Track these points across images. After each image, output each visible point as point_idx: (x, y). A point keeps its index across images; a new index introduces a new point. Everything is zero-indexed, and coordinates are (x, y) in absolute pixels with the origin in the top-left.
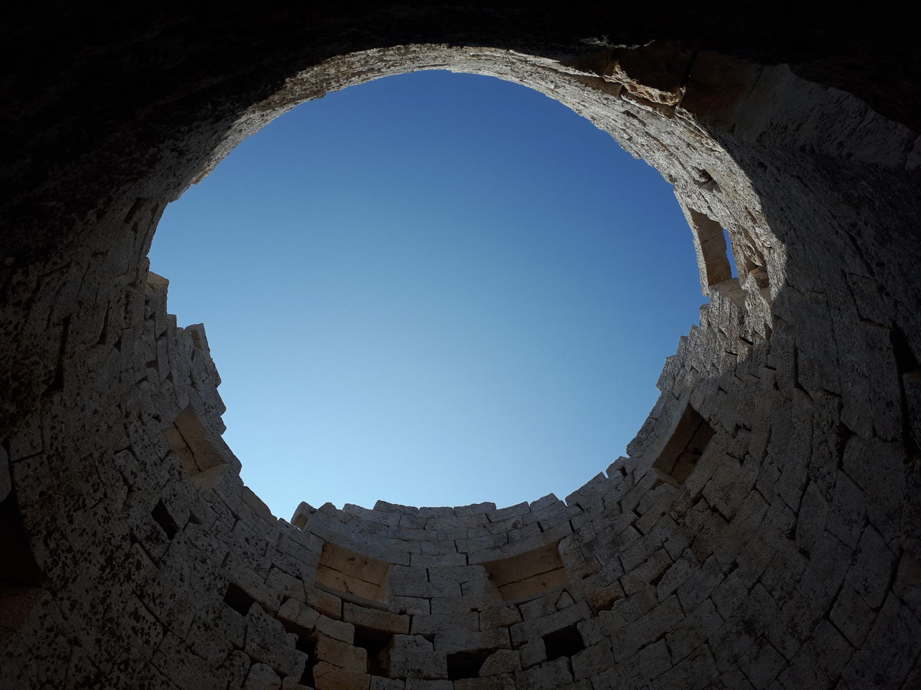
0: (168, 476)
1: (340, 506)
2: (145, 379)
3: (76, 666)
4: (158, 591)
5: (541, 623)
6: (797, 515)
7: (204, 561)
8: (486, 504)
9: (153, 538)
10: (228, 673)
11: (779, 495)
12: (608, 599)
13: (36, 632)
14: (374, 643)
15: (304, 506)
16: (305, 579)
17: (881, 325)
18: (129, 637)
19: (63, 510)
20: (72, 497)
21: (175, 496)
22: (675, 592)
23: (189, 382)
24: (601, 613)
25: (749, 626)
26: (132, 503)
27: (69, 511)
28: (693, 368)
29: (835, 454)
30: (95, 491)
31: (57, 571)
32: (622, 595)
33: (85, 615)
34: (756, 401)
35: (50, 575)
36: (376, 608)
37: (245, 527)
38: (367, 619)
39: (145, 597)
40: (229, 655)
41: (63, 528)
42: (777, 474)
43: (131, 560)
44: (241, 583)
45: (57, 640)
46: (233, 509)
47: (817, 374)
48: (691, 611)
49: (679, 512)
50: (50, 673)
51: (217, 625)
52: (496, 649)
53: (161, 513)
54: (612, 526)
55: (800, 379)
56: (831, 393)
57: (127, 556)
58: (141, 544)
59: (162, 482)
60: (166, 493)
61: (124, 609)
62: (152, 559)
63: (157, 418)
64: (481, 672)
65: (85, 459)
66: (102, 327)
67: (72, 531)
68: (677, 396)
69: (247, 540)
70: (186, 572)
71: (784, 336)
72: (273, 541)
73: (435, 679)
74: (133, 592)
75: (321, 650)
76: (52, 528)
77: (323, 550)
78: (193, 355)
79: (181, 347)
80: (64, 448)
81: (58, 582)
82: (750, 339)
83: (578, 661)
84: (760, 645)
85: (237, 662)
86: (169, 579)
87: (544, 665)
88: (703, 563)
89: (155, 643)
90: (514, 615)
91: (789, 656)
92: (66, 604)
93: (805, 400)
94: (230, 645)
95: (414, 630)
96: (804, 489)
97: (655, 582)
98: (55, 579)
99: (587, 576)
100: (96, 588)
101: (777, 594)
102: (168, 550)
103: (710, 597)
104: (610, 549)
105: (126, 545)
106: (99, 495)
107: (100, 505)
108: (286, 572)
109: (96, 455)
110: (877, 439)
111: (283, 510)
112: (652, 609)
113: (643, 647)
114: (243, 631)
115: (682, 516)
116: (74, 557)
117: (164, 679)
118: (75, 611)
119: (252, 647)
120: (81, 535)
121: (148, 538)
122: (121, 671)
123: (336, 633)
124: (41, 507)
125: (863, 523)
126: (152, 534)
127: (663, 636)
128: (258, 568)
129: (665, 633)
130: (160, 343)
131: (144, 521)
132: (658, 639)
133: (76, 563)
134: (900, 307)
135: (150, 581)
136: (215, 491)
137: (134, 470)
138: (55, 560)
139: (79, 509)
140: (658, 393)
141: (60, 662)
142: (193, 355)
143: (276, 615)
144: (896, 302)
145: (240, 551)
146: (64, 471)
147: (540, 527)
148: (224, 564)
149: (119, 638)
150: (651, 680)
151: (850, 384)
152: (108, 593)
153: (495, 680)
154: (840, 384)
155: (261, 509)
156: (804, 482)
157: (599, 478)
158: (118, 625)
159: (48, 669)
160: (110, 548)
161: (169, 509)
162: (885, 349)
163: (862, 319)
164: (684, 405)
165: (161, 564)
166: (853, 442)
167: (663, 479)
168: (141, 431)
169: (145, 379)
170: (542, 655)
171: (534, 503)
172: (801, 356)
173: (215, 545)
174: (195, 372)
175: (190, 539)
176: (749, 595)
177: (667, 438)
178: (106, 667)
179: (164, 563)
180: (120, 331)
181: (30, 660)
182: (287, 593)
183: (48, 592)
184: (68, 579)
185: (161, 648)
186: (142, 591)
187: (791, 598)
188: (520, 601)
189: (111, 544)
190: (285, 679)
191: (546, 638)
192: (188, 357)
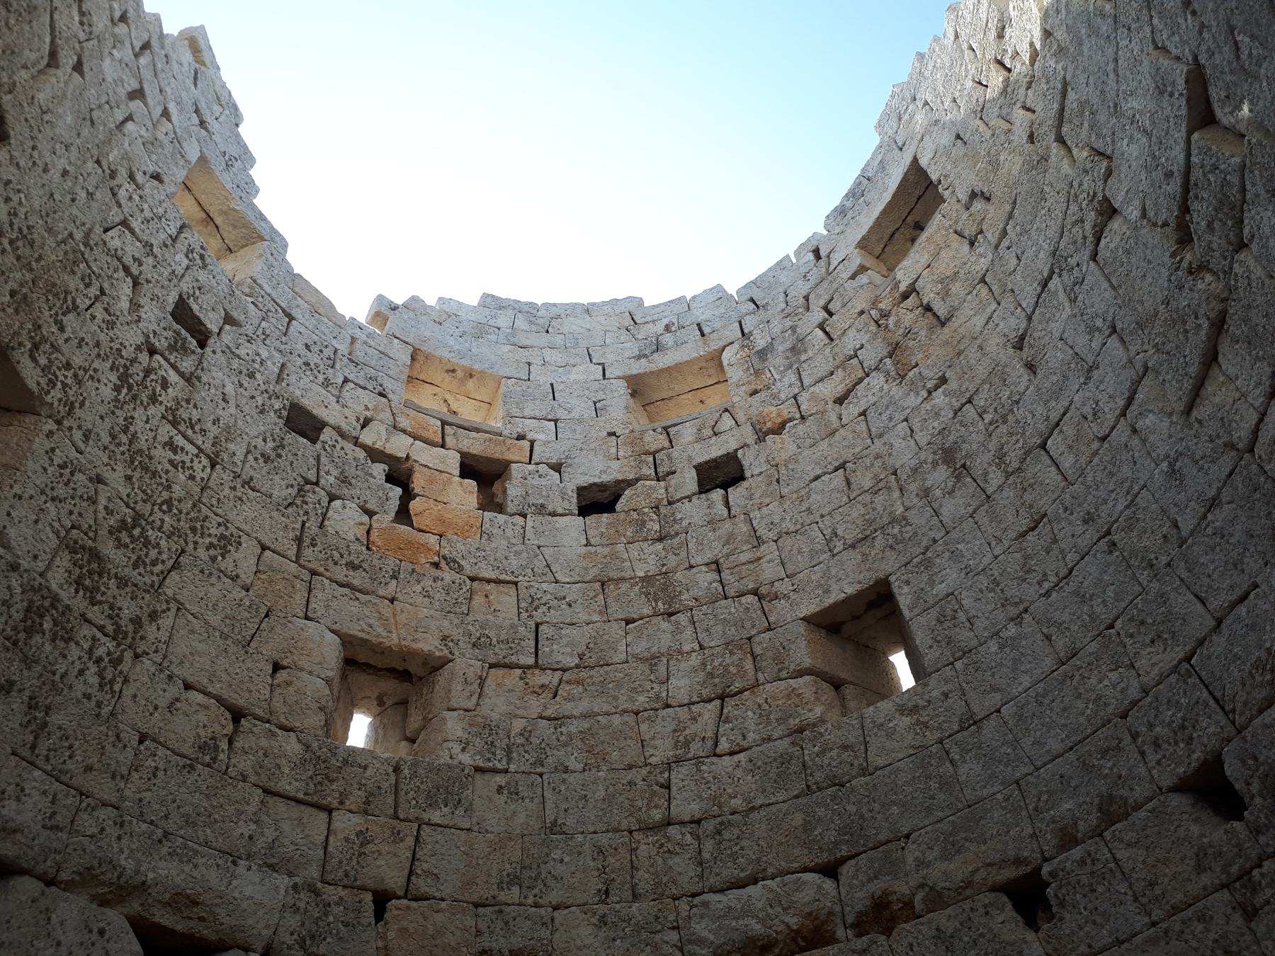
0: (186, 262)
1: (431, 301)
2: (130, 118)
3: (106, 508)
4: (195, 415)
5: (694, 450)
6: (1029, 318)
7: (251, 375)
8: (630, 299)
9: (177, 346)
10: (301, 512)
11: (1013, 291)
12: (780, 420)
13: (45, 469)
14: (485, 474)
15: (380, 298)
16: (390, 396)
17: (1178, 58)
18: (167, 472)
19: (47, 314)
20: (56, 295)
21: (200, 289)
22: (863, 413)
23: (196, 120)
24: (770, 438)
25: (948, 456)
26: (142, 301)
27: (57, 314)
28: (926, 103)
29: (1090, 239)
30: (88, 286)
31: (56, 394)
32: (798, 416)
33: (105, 448)
34: (1002, 158)
35: (48, 399)
36: (486, 432)
37: (302, 329)
38: (475, 445)
39: (179, 423)
40: (299, 491)
41: (52, 339)
42: (1015, 261)
43: (153, 377)
44: (306, 402)
45: (75, 478)
46: (283, 305)
47: (1086, 125)
48: (881, 436)
49: (881, 310)
50: (73, 517)
51: (279, 456)
52: (638, 480)
53: (182, 312)
54: (793, 329)
55: (1064, 129)
56: (1101, 154)
57: (148, 372)
58: (162, 355)
59: (179, 270)
60: (186, 286)
61: (155, 438)
62: (182, 374)
63: (156, 177)
64: (618, 507)
65: (64, 242)
66: (48, 40)
67: (66, 341)
68: (900, 144)
69: (307, 346)
70: (230, 389)
71: (1052, 63)
72: (343, 348)
73: (562, 515)
74: (163, 417)
75: (418, 483)
76: (38, 338)
77: (413, 359)
78: (196, 78)
79: (175, 66)
80: (29, 228)
81: (61, 408)
82: (1008, 63)
83: (736, 494)
84: (958, 478)
85: (311, 498)
86: (208, 399)
87: (694, 499)
88: (903, 377)
89: (202, 479)
90: (662, 440)
91: (990, 490)
92: (77, 435)
93: (1065, 161)
94: (300, 479)
95: (535, 458)
96: (1045, 285)
97: (840, 401)
98: (56, 404)
99: (755, 392)
100: (113, 413)
101: (988, 417)
102: (200, 362)
103: (906, 420)
104: (788, 358)
105: (144, 357)
106: (93, 291)
107: (97, 304)
108: (365, 388)
109: (78, 236)
110: (1145, 222)
111: (353, 305)
112: (833, 433)
113: (817, 478)
114: (314, 462)
115: (885, 315)
116: (75, 375)
117: (221, 520)
118: (91, 442)
119: (329, 480)
120: (80, 346)
121: (172, 348)
122: (164, 512)
123: (436, 464)
124: (17, 311)
125: (1107, 333)
126: (176, 342)
127: (842, 466)
128: (327, 383)
129: (845, 462)
130: (143, 61)
131: (162, 325)
132: (836, 470)
133: (80, 383)
134: (1206, 35)
135: (183, 403)
136: (255, 281)
137: (137, 255)
138: (50, 380)
139: (68, 311)
140: (876, 140)
141: (85, 504)
142: (196, 78)
143: (356, 441)
144: (1203, 26)
145: (299, 362)
146: (37, 260)
147: (700, 329)
148: (279, 379)
149: (155, 474)
150: (822, 516)
151: (1125, 142)
152: (130, 420)
153: (635, 515)
154: (1113, 141)
155: (321, 307)
156: (1045, 275)
157: (782, 265)
158: (151, 458)
159: (71, 513)
160: (123, 362)
161: (195, 307)
162: (1176, 95)
163: (1157, 48)
164: (907, 160)
165: (194, 380)
166: (1116, 224)
167: (868, 265)
168: (136, 197)
169: (130, 118)
170: (695, 488)
171: (694, 297)
172: (1071, 96)
173: (264, 354)
174: (202, 105)
175: (228, 347)
176: (954, 418)
177: (880, 207)
178: (145, 509)
179: (199, 379)
180: (77, 45)
181: (45, 502)
182: (368, 414)
183: (50, 421)
184: (72, 403)
185: (210, 484)
186: (174, 416)
187: (1005, 422)
188: (669, 423)
189: (122, 357)
190: (375, 517)
191: (699, 468)
192: (190, 82)
